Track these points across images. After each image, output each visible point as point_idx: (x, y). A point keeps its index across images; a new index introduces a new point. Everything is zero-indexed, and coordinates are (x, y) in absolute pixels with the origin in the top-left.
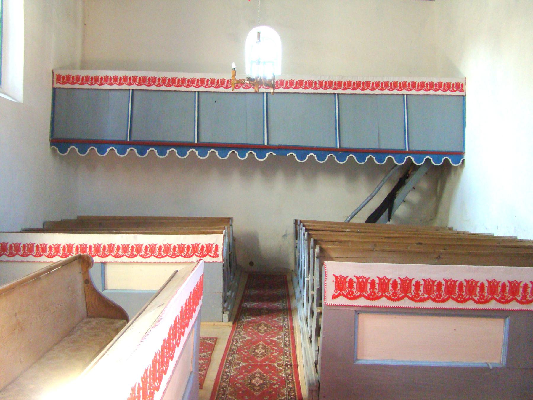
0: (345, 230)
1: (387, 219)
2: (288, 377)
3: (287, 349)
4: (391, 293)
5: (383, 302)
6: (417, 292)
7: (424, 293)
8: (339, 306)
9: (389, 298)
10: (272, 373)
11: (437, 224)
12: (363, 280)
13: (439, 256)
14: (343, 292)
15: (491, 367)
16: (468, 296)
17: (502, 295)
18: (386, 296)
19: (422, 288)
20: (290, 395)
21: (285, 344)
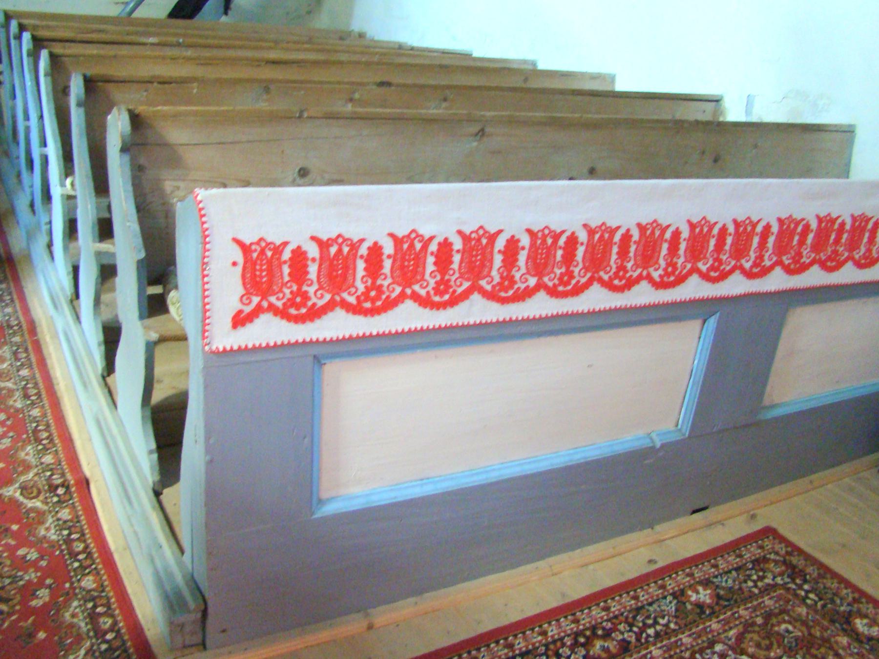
0: (143, 40)
1: (222, 10)
2: (68, 541)
3: (36, 412)
4: (432, 283)
5: (408, 317)
6: (510, 271)
7: (528, 273)
8: (256, 349)
9: (425, 302)
10: (15, 535)
11: (323, 21)
12: (340, 251)
13: (482, 130)
14: (273, 299)
15: (658, 445)
16: (639, 271)
17: (715, 260)
18: (415, 297)
19: (522, 257)
20: (100, 634)
21: (26, 396)
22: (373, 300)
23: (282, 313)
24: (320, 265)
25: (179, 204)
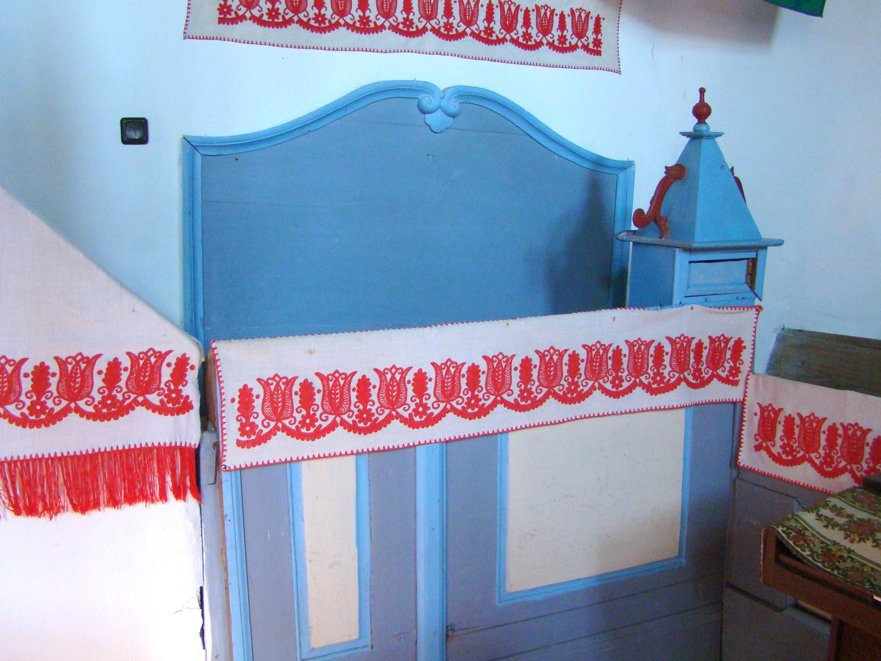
4: (413, 406)
22: (659, 383)
23: (463, 414)
24: (324, 394)
25: (30, 372)
